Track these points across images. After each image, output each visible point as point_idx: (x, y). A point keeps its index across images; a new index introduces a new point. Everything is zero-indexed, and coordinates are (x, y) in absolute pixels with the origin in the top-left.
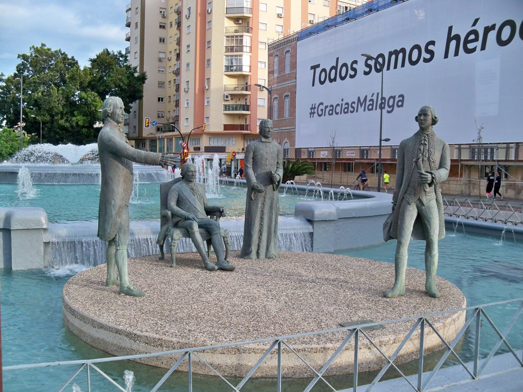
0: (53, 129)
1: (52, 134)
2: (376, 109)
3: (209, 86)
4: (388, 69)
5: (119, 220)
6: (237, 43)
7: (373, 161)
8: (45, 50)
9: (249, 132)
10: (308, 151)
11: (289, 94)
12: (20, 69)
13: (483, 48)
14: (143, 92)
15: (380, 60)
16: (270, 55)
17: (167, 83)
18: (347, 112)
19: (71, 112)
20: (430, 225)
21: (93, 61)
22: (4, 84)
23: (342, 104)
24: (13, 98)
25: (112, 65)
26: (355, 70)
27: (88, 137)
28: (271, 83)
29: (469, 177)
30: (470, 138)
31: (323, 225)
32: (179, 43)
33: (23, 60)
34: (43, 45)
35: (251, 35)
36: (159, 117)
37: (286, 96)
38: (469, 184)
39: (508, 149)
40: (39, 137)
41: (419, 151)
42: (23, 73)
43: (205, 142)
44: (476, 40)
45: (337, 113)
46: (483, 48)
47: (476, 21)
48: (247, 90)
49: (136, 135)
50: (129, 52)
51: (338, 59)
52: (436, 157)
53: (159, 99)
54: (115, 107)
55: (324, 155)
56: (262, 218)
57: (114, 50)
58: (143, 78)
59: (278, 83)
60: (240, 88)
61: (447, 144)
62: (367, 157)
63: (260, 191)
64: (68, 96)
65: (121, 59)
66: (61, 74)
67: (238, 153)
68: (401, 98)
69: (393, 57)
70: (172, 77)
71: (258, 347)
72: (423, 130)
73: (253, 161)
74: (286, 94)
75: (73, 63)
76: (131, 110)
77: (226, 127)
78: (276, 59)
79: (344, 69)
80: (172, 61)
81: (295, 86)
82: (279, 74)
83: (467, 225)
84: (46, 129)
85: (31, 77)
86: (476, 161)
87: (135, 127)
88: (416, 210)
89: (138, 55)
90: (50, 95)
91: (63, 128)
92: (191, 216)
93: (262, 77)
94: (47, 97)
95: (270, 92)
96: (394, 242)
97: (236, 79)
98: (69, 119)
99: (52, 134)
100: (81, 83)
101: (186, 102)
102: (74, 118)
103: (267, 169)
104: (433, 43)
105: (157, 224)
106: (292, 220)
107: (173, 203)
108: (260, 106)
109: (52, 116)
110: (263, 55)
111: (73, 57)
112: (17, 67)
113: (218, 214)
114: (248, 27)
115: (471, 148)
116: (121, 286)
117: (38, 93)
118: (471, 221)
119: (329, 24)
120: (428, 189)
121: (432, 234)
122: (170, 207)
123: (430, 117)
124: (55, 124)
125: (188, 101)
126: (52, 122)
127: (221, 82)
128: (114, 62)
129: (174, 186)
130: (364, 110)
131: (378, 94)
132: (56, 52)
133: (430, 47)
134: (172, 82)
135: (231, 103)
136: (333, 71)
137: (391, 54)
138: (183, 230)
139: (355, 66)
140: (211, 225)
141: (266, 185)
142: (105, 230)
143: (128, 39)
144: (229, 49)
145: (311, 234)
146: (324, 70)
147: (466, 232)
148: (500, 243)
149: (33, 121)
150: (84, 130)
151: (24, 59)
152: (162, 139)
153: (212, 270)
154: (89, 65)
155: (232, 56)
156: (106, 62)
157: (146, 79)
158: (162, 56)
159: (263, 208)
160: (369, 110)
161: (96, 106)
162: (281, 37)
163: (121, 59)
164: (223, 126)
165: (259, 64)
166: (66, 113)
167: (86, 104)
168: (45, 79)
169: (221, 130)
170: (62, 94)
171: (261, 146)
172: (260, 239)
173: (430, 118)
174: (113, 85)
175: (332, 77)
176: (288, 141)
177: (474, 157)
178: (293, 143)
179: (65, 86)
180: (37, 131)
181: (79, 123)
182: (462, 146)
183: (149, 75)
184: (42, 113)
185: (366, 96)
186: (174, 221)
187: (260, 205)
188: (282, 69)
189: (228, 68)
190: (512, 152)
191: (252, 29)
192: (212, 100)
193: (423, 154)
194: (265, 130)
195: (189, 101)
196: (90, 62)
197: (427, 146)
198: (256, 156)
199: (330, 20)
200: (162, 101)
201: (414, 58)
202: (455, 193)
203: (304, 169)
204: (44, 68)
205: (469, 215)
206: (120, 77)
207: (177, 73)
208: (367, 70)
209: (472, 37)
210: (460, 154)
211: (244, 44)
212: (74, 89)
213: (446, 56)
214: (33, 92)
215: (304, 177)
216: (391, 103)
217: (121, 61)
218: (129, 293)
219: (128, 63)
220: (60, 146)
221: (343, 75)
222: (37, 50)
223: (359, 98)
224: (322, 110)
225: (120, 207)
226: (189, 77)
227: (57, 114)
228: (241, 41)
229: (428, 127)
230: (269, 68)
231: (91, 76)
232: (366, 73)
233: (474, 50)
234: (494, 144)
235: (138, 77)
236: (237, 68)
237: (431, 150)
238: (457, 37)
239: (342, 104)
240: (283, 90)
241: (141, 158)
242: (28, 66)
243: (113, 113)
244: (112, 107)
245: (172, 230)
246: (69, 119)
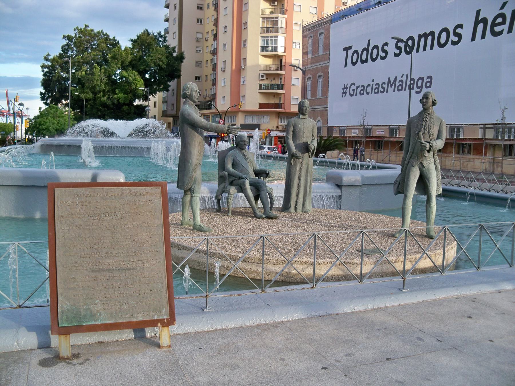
1: (94, 111)
2: (405, 90)
3: (245, 66)
4: (418, 51)
5: (195, 174)
6: (272, 24)
7: (401, 140)
8: (89, 31)
9: (283, 110)
10: (340, 129)
11: (322, 74)
12: (65, 49)
13: (510, 31)
14: (181, 71)
15: (410, 43)
16: (304, 37)
17: (204, 62)
18: (378, 92)
19: (112, 90)
20: (429, 183)
21: (134, 41)
22: (50, 64)
23: (373, 85)
24: (59, 76)
25: (152, 45)
26: (385, 52)
27: (128, 114)
28: (305, 63)
29: (494, 155)
30: (494, 119)
31: (350, 190)
32: (216, 24)
33: (67, 41)
34: (87, 26)
35: (285, 16)
37: (319, 76)
38: (493, 162)
40: (82, 113)
42: (67, 53)
43: (240, 120)
44: (504, 23)
45: (368, 93)
46: (510, 31)
47: (504, 4)
48: (281, 70)
49: (174, 112)
50: (168, 33)
51: (369, 41)
52: (435, 131)
53: (196, 78)
54: (192, 90)
55: (355, 133)
56: (299, 180)
57: (155, 30)
58: (181, 58)
59: (311, 64)
60: (275, 68)
62: (396, 135)
63: (298, 158)
64: (110, 74)
65: (160, 39)
66: (103, 54)
67: (273, 130)
68: (429, 80)
69: (423, 39)
70: (209, 57)
71: (298, 260)
72: (425, 110)
74: (319, 74)
75: (115, 44)
76: (169, 88)
77: (261, 105)
78: (310, 41)
79: (375, 51)
80: (209, 41)
81: (328, 67)
82: (313, 55)
83: (478, 195)
84: (89, 106)
85: (75, 56)
87: (173, 104)
88: (419, 171)
89: (176, 36)
90: (93, 74)
91: (104, 105)
92: (244, 176)
93: (296, 57)
94: (90, 76)
95: (304, 72)
96: (402, 195)
97: (272, 59)
98: (111, 97)
99: (94, 111)
100: (122, 63)
101: (223, 81)
102: (115, 96)
103: (304, 140)
104: (460, 26)
105: (215, 185)
106: (324, 184)
107: (229, 166)
108: (294, 85)
109: (95, 93)
110: (298, 36)
111: (114, 38)
112: (62, 48)
113: (265, 175)
114: (283, 8)
115: (496, 127)
116: (195, 224)
117: (81, 72)
118: (485, 192)
119: (362, 7)
120: (427, 154)
121: (431, 190)
122: (227, 169)
123: (431, 100)
125: (224, 79)
126: (95, 99)
127: (257, 60)
128: (154, 42)
129: (230, 153)
130: (394, 91)
131: (407, 75)
132: (98, 32)
133: (459, 30)
134: (209, 61)
135: (266, 82)
136: (365, 53)
137: (420, 37)
138: (237, 187)
139: (385, 48)
140: (259, 183)
141: (303, 153)
142: (184, 182)
143: (167, 20)
144: (265, 30)
145: (340, 197)
146: (356, 52)
147: (477, 202)
148: (505, 211)
149: (76, 99)
150: (125, 108)
151: (68, 39)
153: (260, 218)
154: (130, 45)
155: (267, 37)
156: (146, 42)
157: (184, 59)
158: (199, 36)
160: (399, 90)
161: (136, 85)
162: (315, 19)
163: (160, 39)
164: (258, 104)
165: (294, 45)
166: (108, 91)
167: (127, 82)
168: (88, 59)
169: (256, 108)
170: (104, 73)
171: (299, 121)
174: (153, 65)
175: (364, 58)
176: (321, 120)
177: (454, 136)
178: (325, 122)
179: (107, 65)
181: (120, 101)
182: (487, 126)
183: (186, 55)
184: (86, 91)
185: (396, 78)
186: (229, 178)
187: (298, 169)
188: (315, 50)
189: (264, 49)
191: (287, 10)
192: (248, 79)
193: (424, 128)
194: (303, 109)
195: (226, 80)
196: (131, 43)
197: (428, 122)
198: (295, 130)
199: (363, 3)
200: (199, 79)
201: (443, 41)
203: (336, 145)
204: (87, 48)
206: (160, 56)
207: (214, 52)
208: (397, 52)
209: (500, 20)
210: (484, 134)
211: (279, 25)
212: (116, 68)
213: (473, 39)
214: (76, 71)
215: (336, 152)
216: (420, 84)
217: (160, 41)
218: (200, 229)
219: (167, 44)
220: (110, 121)
221: (374, 56)
222: (81, 31)
223: (389, 79)
224: (354, 90)
225: (196, 165)
226: (226, 57)
227: (100, 92)
228: (277, 22)
230: (303, 49)
231: (132, 55)
232: (396, 55)
233: (501, 33)
235: (177, 56)
236: (272, 49)
238: (485, 21)
239: (373, 85)
240: (317, 70)
241: (212, 128)
242: (73, 46)
243: (191, 95)
244: (190, 90)
245: (229, 187)
246: (111, 97)
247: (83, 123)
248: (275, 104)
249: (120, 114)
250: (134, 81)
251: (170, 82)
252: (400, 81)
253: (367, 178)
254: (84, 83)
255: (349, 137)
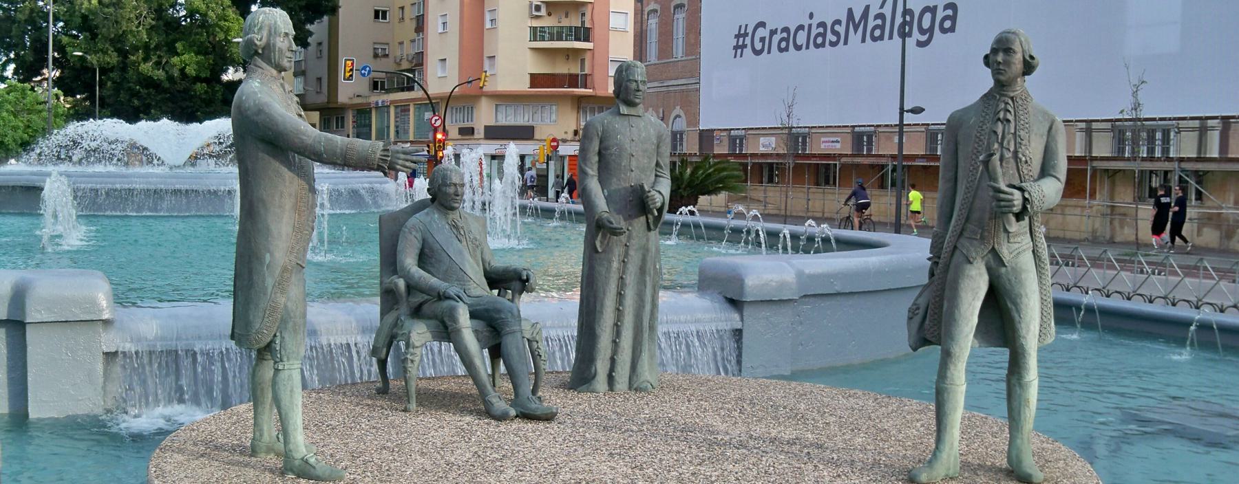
0: (126, 85)
1: (123, 96)
2: (891, 37)
7: (883, 161)
9: (589, 91)
10: (730, 136)
18: (823, 45)
19: (167, 44)
20: (1018, 312)
23: (810, 26)
24: (32, 10)
27: (209, 102)
29: (1112, 198)
30: (1115, 107)
31: (765, 312)
36: (376, 56)
37: (677, 7)
38: (1112, 214)
39: (1203, 131)
40: (93, 103)
41: (994, 137)
43: (485, 115)
45: (798, 48)
49: (322, 99)
52: (1034, 152)
54: (273, 32)
55: (766, 145)
56: (620, 296)
61: (1059, 119)
62: (870, 150)
63: (615, 232)
64: (160, 5)
67: (564, 141)
68: (950, 12)
72: (1001, 86)
73: (600, 161)
76: (309, 40)
77: (536, 80)
83: (1106, 313)
84: (109, 84)
86: (1128, 159)
87: (320, 79)
88: (986, 278)
91: (148, 82)
92: (453, 290)
94: (111, 10)
96: (936, 350)
98: (164, 60)
99: (123, 96)
101: (440, 21)
102: (175, 60)
103: (633, 179)
105: (372, 309)
107: (410, 262)
108: (616, 30)
109: (123, 54)
113: (517, 285)
115: (1117, 128)
116: (287, 455)
118: (1116, 303)
120: (1014, 226)
121: (1023, 332)
122: (403, 269)
123: (1019, 56)
124: (131, 72)
126: (124, 67)
129: (413, 220)
130: (863, 40)
135: (547, 22)
138: (433, 322)
140: (499, 311)
141: (629, 218)
145: (738, 334)
147: (1104, 328)
148: (1183, 356)
149: (78, 65)
150: (200, 87)
152: (383, 109)
153: (502, 418)
159: (624, 272)
160: (874, 39)
161: (227, 31)
164: (528, 78)
166: (157, 48)
167: (204, 25)
169: (523, 86)
171: (618, 124)
172: (615, 344)
173: (1018, 58)
176: (682, 114)
177: (1124, 152)
178: (693, 119)
180: (89, 88)
181: (188, 70)
182: (1094, 125)
184: (100, 46)
185: (867, 7)
186: (412, 301)
187: (615, 265)
190: (1214, 138)
193: (1001, 144)
194: (627, 88)
195: (448, 19)
197: (1012, 125)
198: (606, 149)
200: (384, 17)
202: (1077, 236)
203: (721, 180)
205: (1112, 288)
210: (1089, 145)
215: (720, 198)
216: (926, 24)
220: (143, 124)
223: (850, 11)
224: (762, 40)
227: (135, 49)
229: (1014, 80)
234: (1170, 119)
237: (1022, 133)
239: (810, 26)
241: (335, 154)
243: (268, 47)
244: (265, 33)
246: (164, 60)
247: (91, 125)
248: (571, 75)
249: (188, 103)
250: (222, 23)
251: (312, 23)
252: (876, 17)
253: (812, 277)
254: (97, 27)
255: (753, 155)
